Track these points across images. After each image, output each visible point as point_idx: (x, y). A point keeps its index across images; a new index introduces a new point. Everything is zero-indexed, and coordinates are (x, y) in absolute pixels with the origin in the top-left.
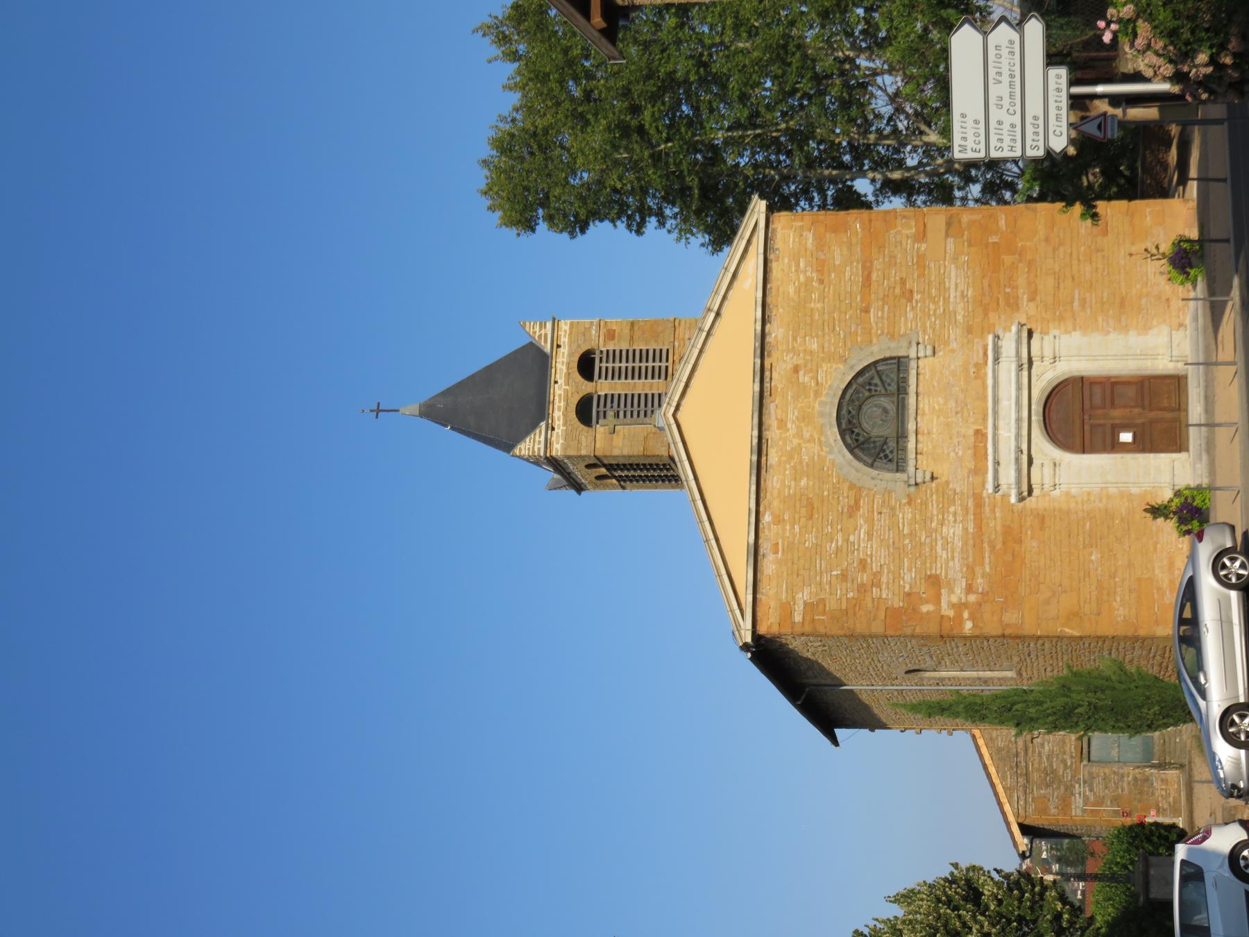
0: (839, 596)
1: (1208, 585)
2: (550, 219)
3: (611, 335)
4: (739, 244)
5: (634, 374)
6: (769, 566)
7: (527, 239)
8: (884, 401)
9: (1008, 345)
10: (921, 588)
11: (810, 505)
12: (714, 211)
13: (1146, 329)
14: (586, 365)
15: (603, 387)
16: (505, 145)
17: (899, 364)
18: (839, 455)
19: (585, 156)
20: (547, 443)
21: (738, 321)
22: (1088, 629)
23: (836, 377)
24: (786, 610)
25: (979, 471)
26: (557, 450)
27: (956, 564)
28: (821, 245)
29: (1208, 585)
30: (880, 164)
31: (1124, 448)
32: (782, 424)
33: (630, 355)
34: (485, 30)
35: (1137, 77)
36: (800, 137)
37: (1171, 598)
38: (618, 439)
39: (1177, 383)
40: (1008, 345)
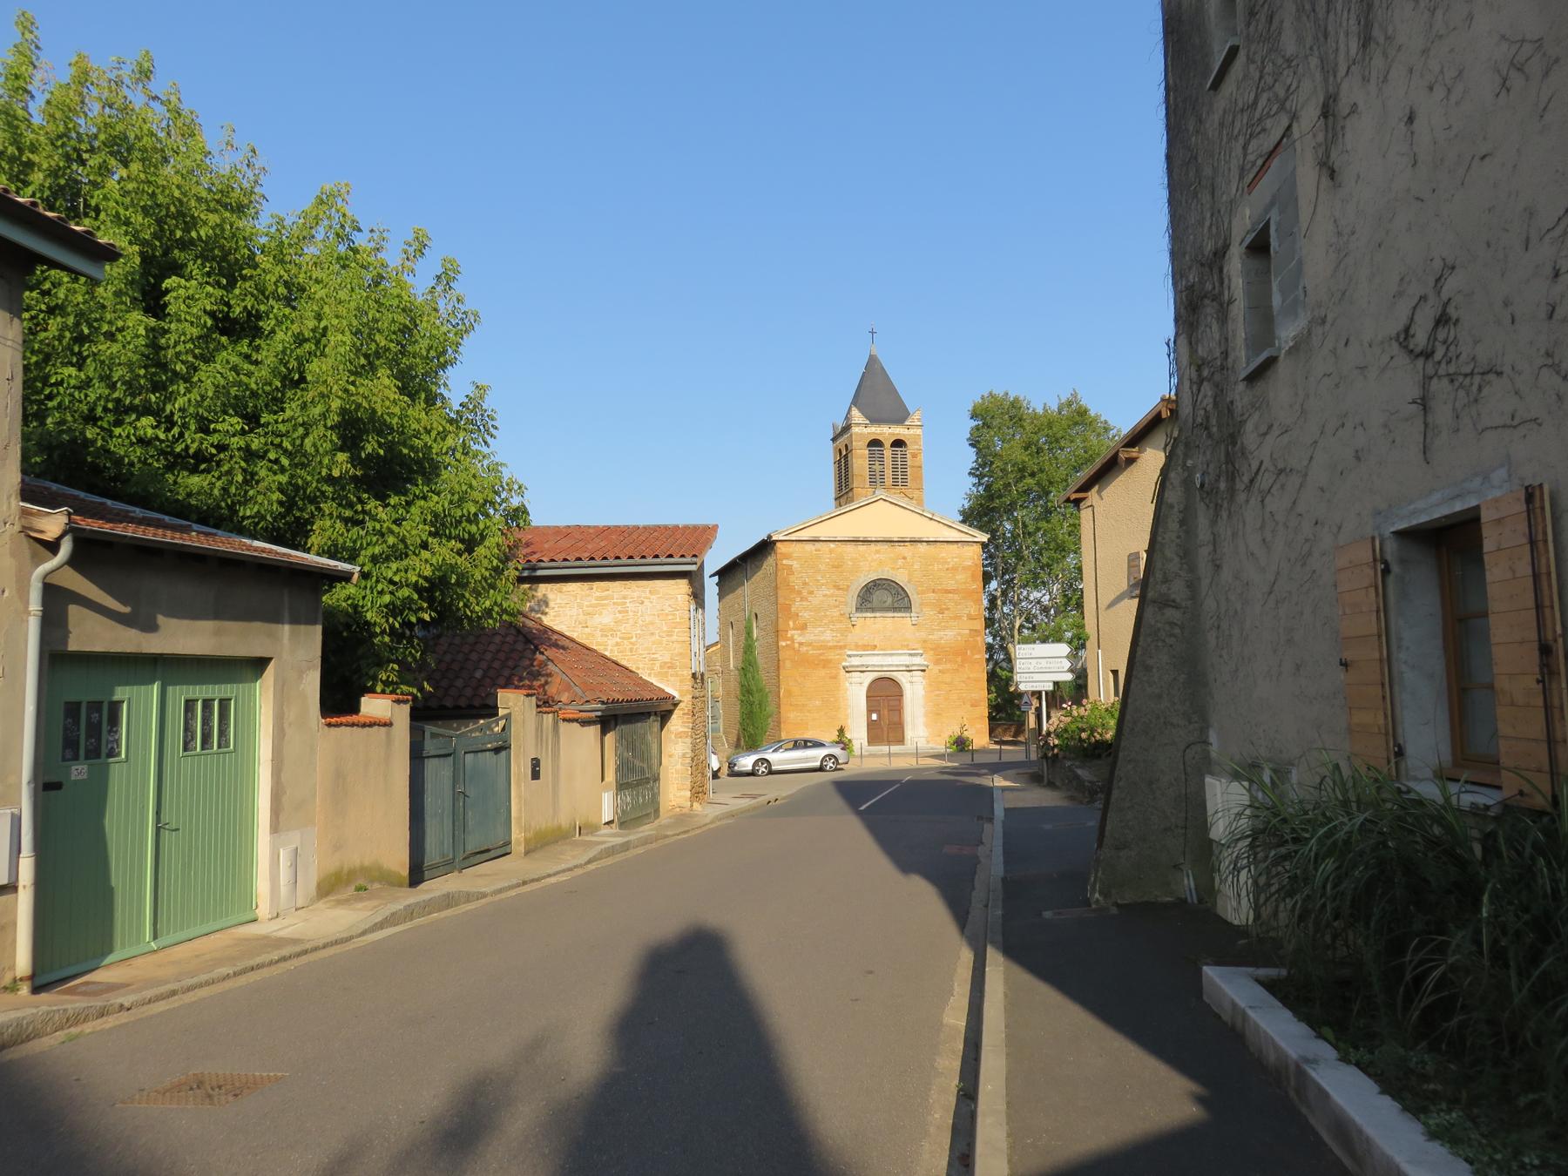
0: (795, 581)
1: (820, 753)
2: (977, 428)
3: (914, 456)
4: (965, 528)
5: (895, 468)
6: (809, 547)
7: (968, 415)
8: (890, 600)
9: (918, 660)
10: (801, 621)
11: (837, 567)
12: (979, 514)
13: (927, 725)
14: (898, 443)
15: (888, 452)
16: (1016, 404)
17: (908, 608)
18: (864, 580)
19: (1010, 449)
20: (858, 424)
21: (925, 525)
22: (783, 701)
23: (901, 578)
24: (788, 556)
25: (857, 647)
26: (855, 430)
27: (812, 638)
28: (965, 569)
29: (820, 753)
30: (1004, 593)
31: (869, 716)
32: (878, 552)
33: (904, 465)
34: (1075, 395)
35: (1049, 717)
36: (1019, 557)
37: (808, 736)
38: (860, 460)
39: (901, 741)
40: (918, 660)
